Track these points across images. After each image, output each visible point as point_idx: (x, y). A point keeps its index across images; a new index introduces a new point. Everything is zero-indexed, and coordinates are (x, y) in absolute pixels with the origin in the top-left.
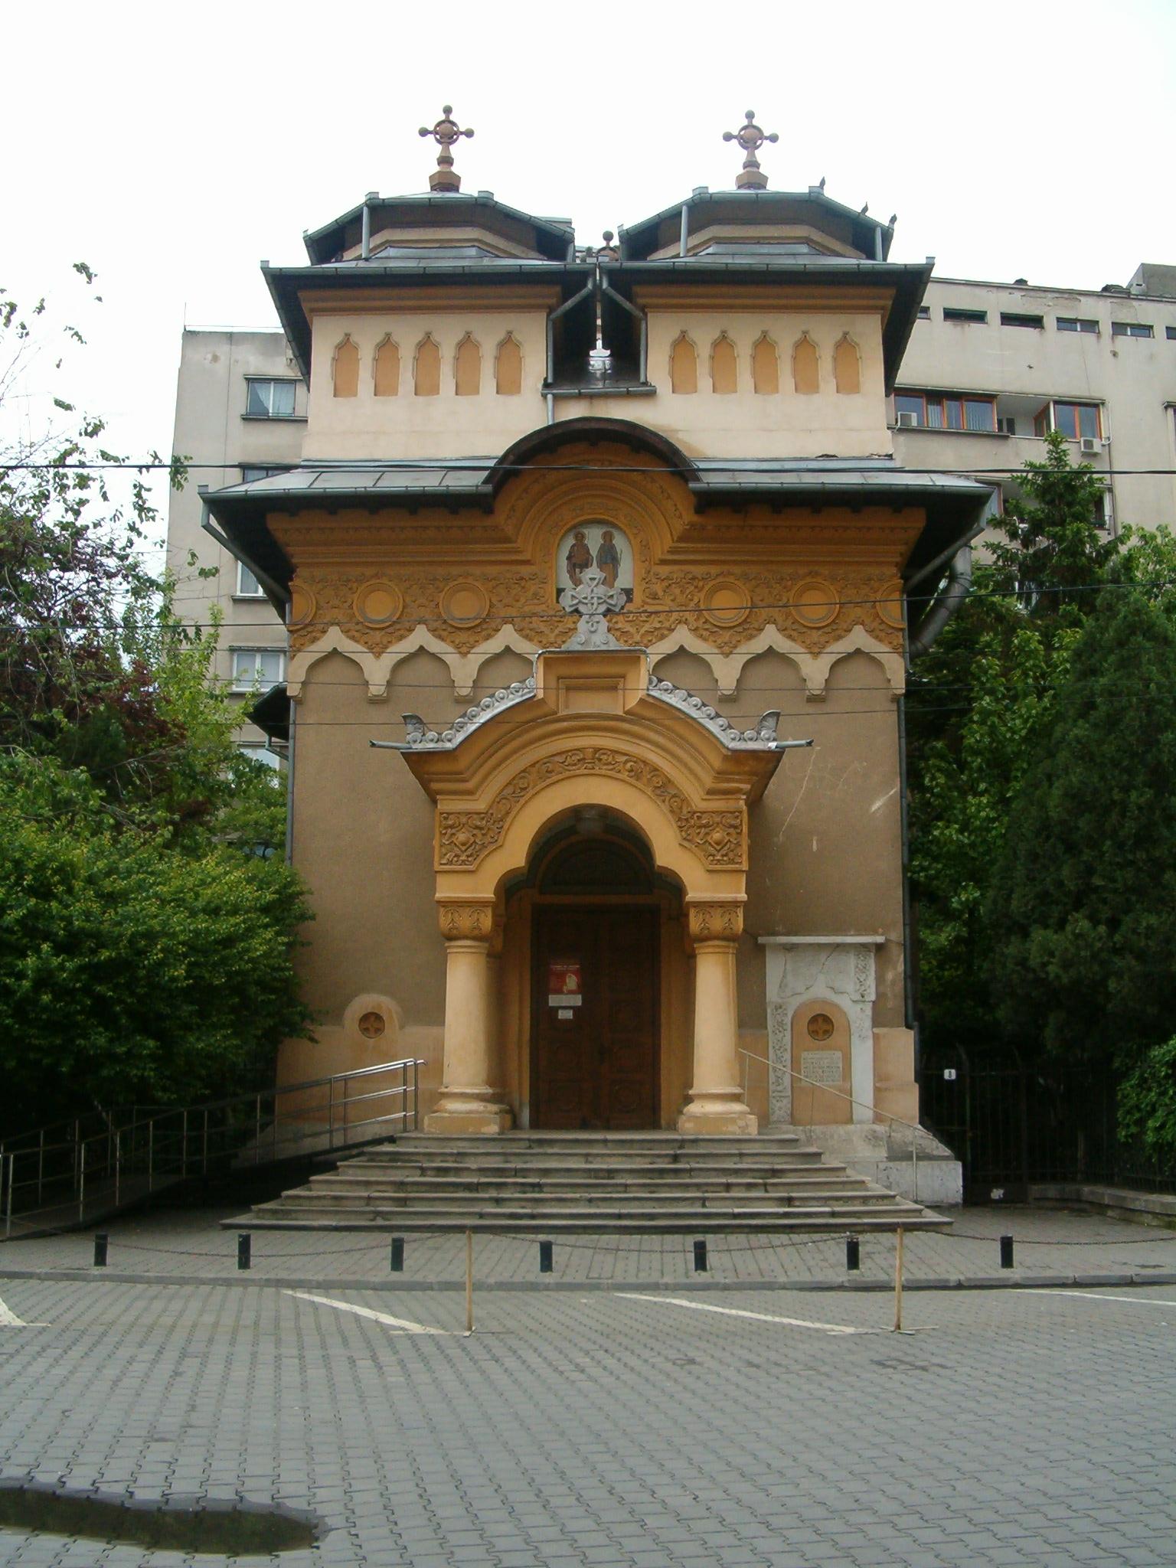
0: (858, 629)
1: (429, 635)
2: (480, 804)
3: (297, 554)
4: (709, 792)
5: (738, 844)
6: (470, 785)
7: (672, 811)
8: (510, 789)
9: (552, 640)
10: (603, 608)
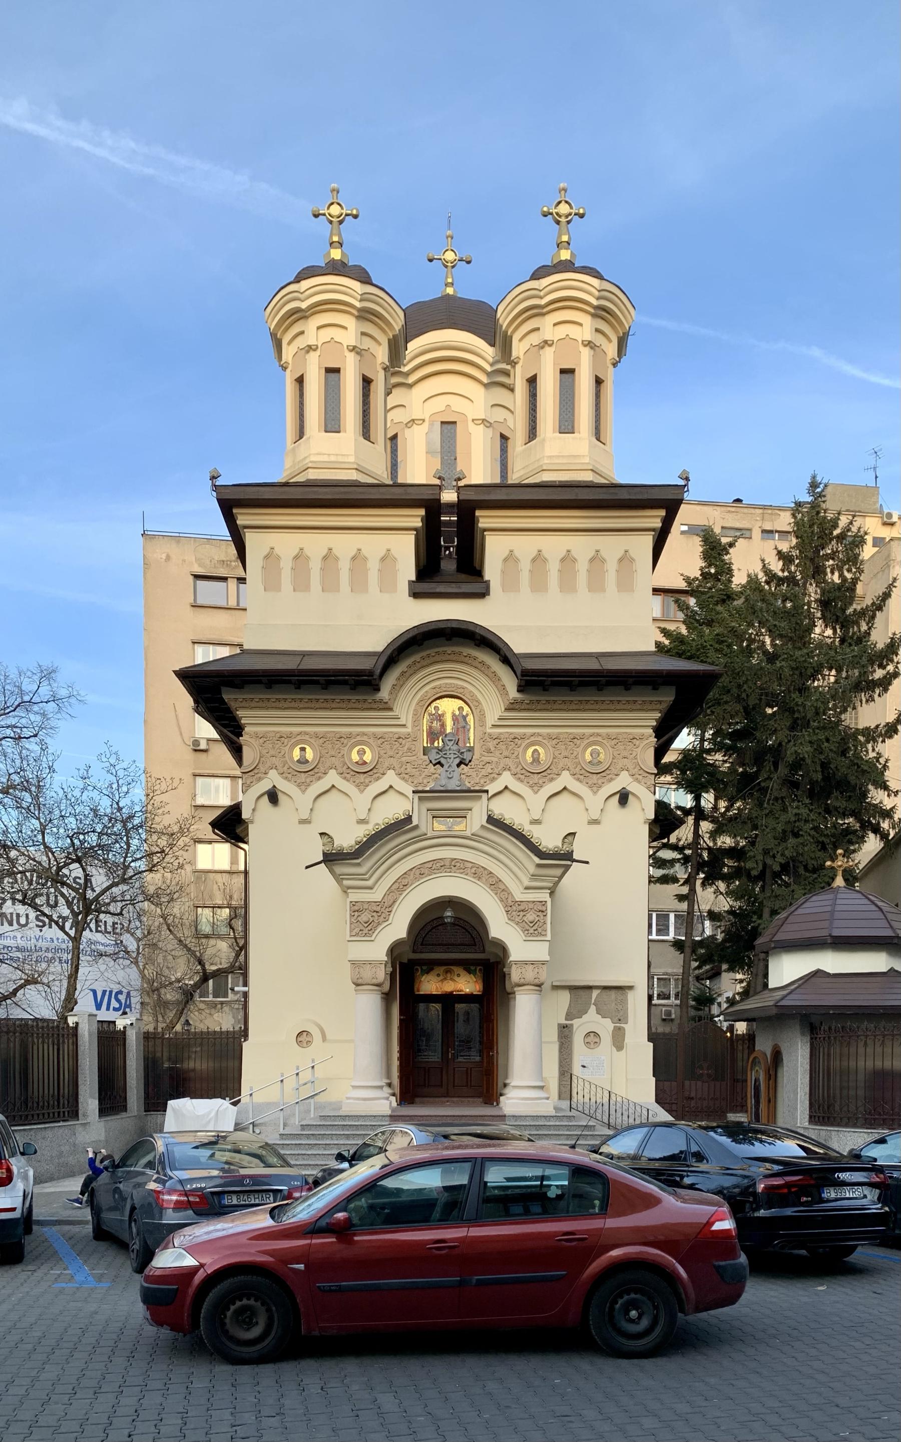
0: (566, 773)
1: (338, 777)
2: (377, 895)
3: (245, 716)
4: (527, 888)
5: (545, 923)
6: (369, 883)
7: (502, 901)
8: (397, 885)
9: (478, 781)
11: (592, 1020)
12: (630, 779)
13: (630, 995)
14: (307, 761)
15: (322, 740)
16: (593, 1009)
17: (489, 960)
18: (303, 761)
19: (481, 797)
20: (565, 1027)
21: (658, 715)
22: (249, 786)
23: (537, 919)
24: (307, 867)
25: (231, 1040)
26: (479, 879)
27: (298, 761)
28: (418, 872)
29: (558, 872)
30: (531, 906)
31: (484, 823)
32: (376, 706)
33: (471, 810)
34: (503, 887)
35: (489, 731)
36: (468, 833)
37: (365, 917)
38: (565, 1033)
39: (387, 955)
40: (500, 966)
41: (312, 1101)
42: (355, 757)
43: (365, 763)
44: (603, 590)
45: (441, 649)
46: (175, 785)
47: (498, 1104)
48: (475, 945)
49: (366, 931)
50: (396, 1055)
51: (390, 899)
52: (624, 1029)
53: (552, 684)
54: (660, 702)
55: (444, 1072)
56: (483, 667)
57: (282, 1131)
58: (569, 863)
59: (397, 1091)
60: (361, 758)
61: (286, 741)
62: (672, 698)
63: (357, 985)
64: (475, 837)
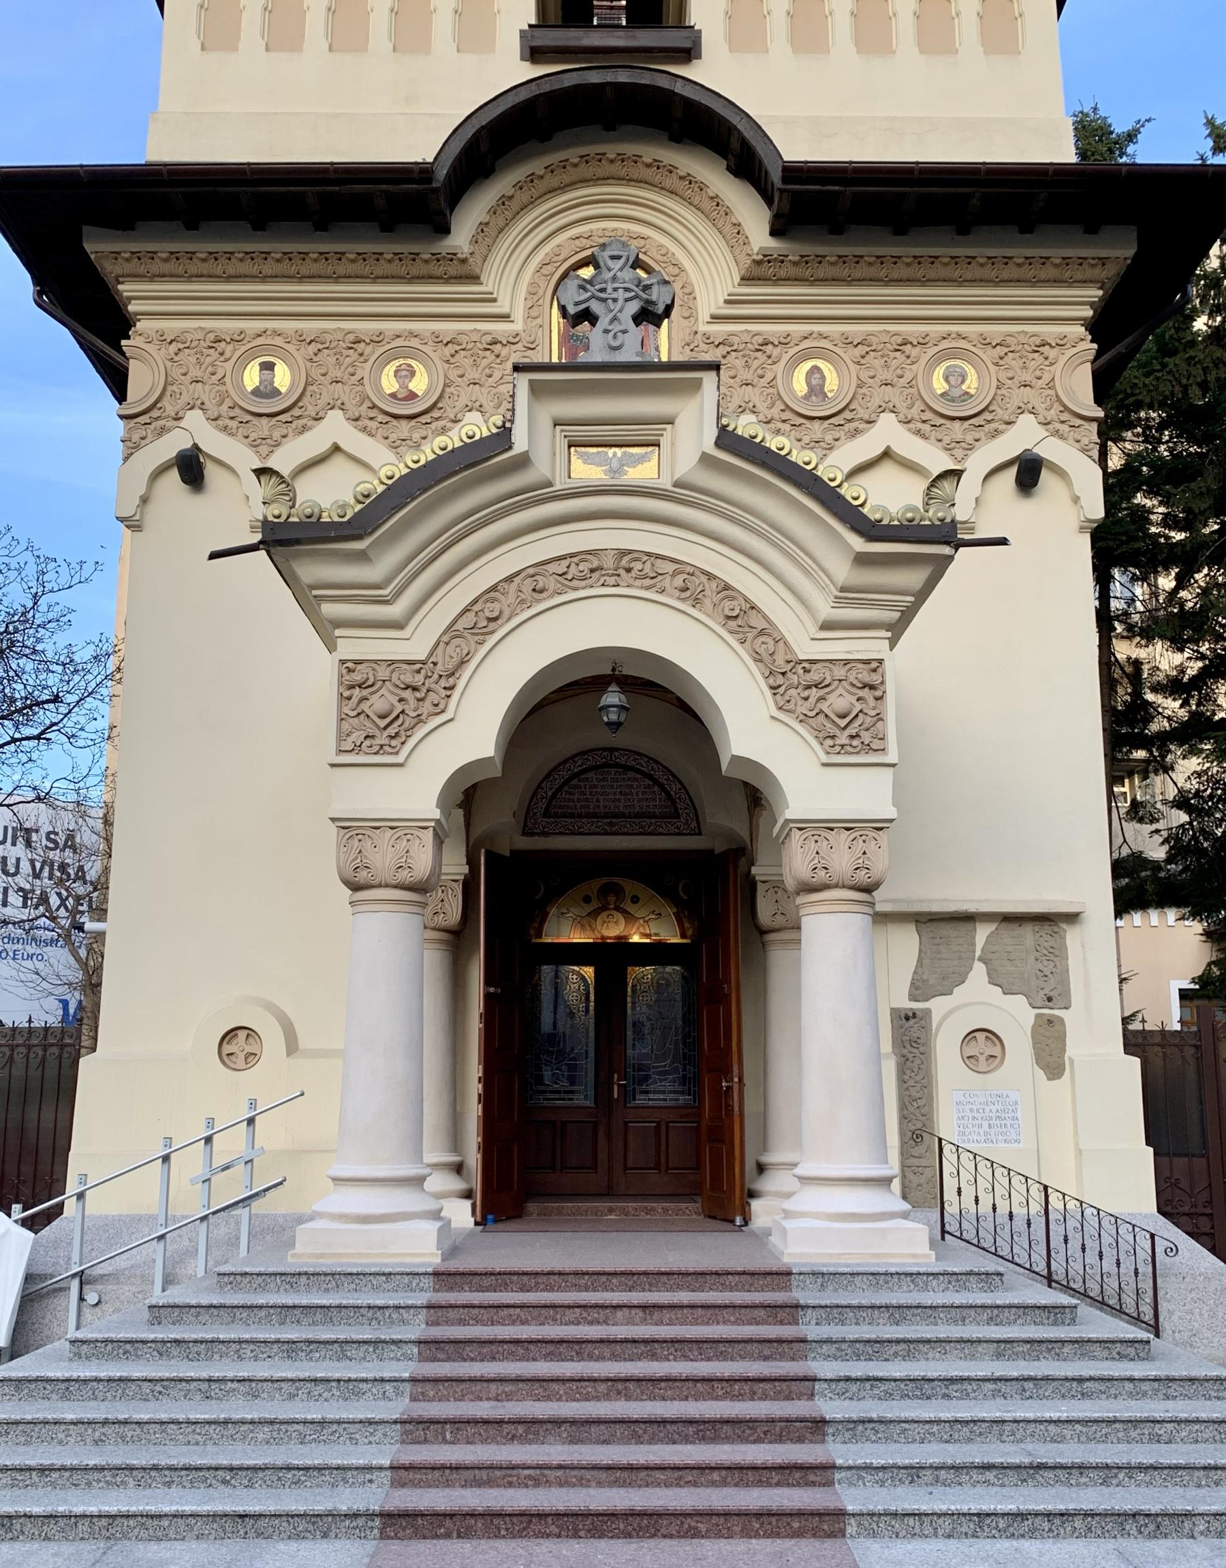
2: (416, 644)
3: (136, 295)
4: (827, 626)
5: (879, 718)
6: (395, 610)
7: (758, 659)
10: (634, 307)
11: (976, 1000)
12: (1042, 432)
13: (1072, 936)
14: (276, 393)
15: (313, 348)
16: (979, 971)
17: (712, 851)
18: (266, 391)
19: (698, 384)
20: (910, 1016)
21: (1096, 293)
22: (137, 447)
23: (858, 706)
24: (214, 556)
25: (55, 1050)
26: (696, 602)
27: (256, 392)
28: (528, 585)
29: (914, 578)
30: (840, 672)
31: (709, 445)
32: (439, 271)
33: (671, 423)
34: (761, 624)
35: (703, 328)
36: (666, 483)
37: (378, 702)
38: (911, 1034)
39: (442, 802)
40: (743, 861)
41: (242, 1212)
42: (389, 383)
43: (412, 396)
44: (950, 49)
45: (591, 150)
46: (85, 574)
47: (746, 1222)
48: (678, 816)
49: (382, 739)
50: (474, 1088)
51: (453, 652)
52: (1062, 1021)
53: (857, 216)
54: (1103, 261)
55: (601, 1133)
56: (688, 190)
57: (72, 1334)
58: (947, 550)
59: (477, 1186)
60: (404, 386)
61: (229, 348)
62: (1130, 252)
63: (356, 887)
64: (682, 492)
